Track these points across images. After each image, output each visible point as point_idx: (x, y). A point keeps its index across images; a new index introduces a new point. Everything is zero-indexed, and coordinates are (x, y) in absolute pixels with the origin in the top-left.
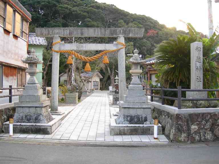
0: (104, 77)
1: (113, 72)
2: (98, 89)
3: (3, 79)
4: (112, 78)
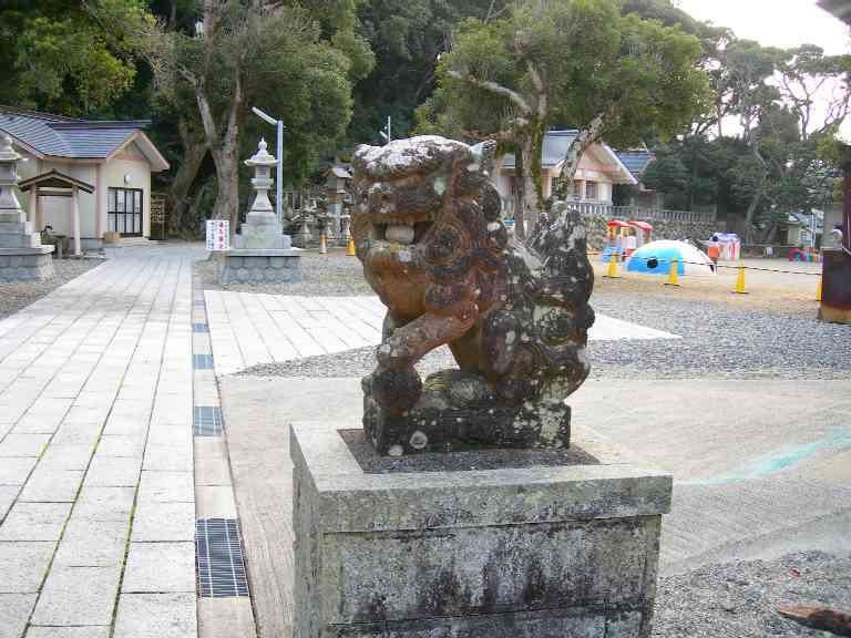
0: (175, 165)
1: (233, 130)
2: (140, 234)
3: (77, 178)
4: (226, 164)
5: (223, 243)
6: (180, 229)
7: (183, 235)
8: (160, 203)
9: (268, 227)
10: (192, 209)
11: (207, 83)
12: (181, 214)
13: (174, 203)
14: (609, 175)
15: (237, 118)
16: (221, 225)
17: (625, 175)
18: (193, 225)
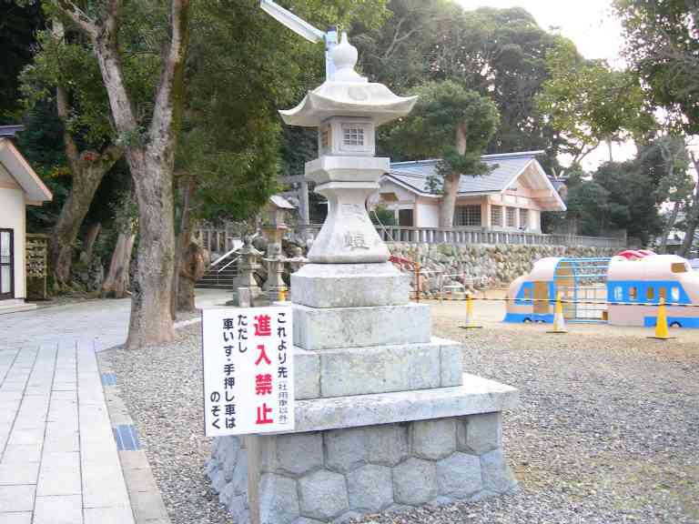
0: (62, 183)
2: (11, 295)
5: (271, 400)
6: (69, 283)
7: (72, 291)
8: (40, 249)
9: (386, 311)
10: (83, 255)
11: (117, 30)
12: (69, 262)
13: (60, 248)
14: (537, 201)
15: (172, 93)
16: (263, 326)
17: (556, 201)
18: (85, 277)
